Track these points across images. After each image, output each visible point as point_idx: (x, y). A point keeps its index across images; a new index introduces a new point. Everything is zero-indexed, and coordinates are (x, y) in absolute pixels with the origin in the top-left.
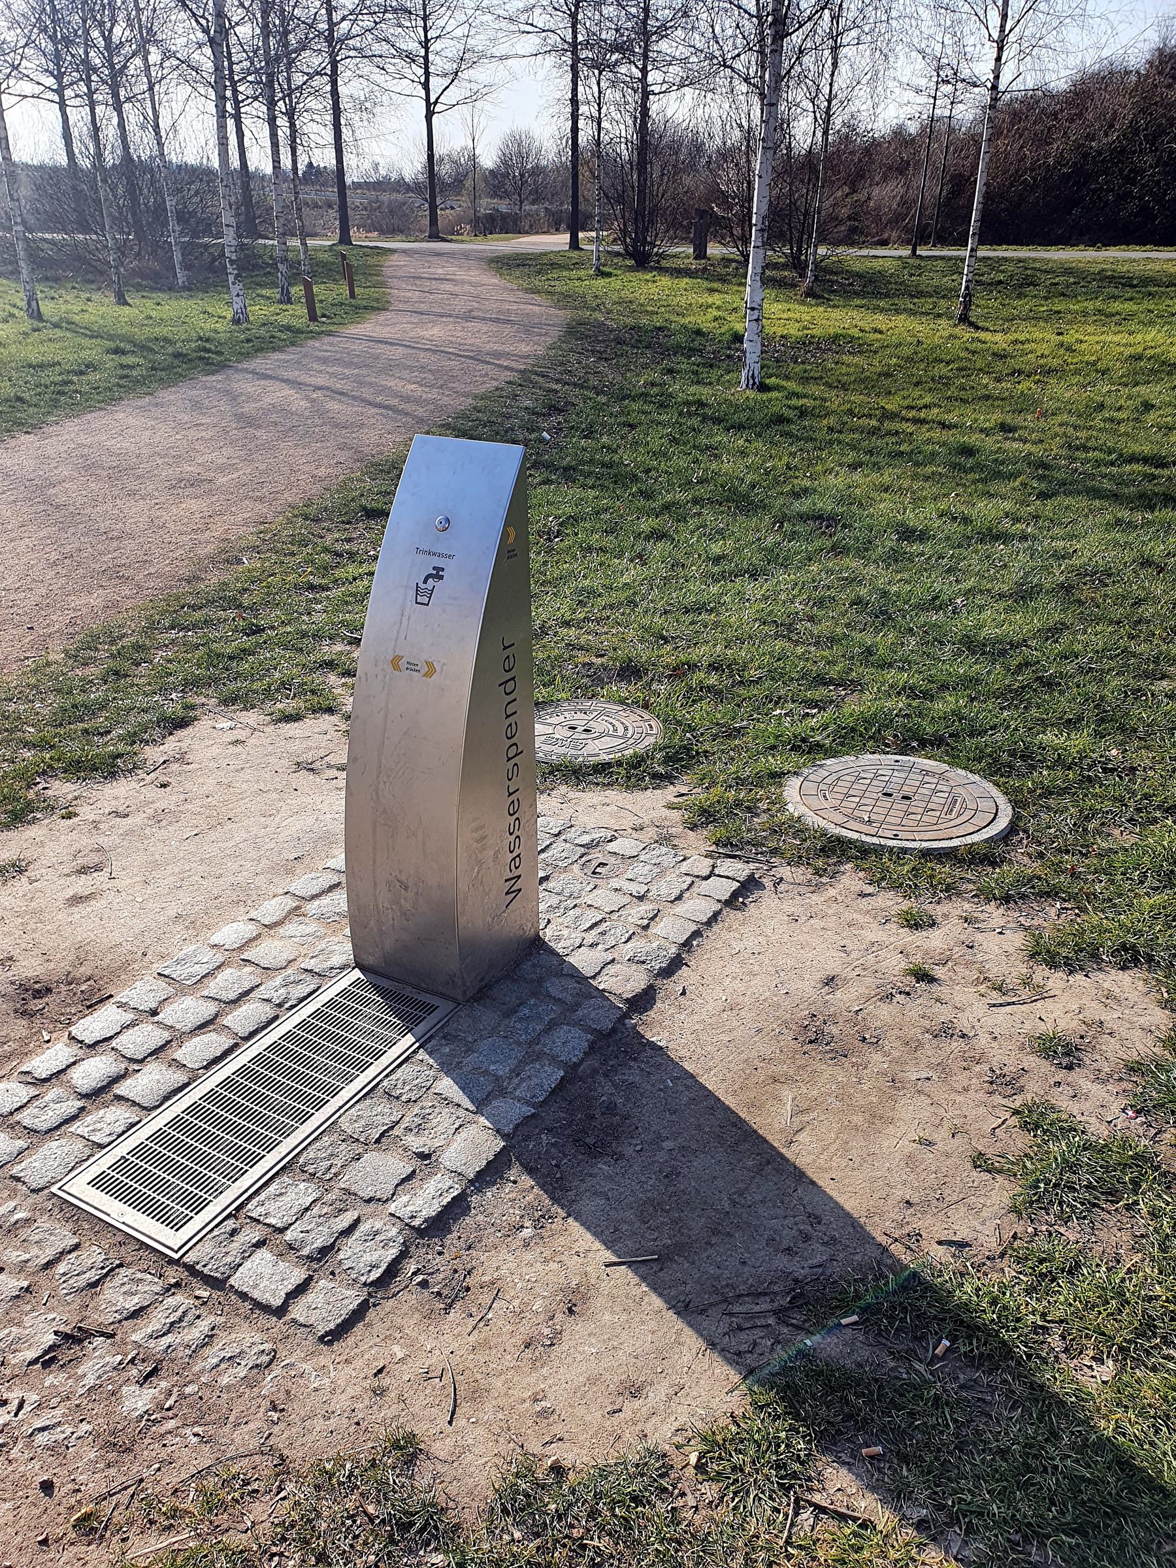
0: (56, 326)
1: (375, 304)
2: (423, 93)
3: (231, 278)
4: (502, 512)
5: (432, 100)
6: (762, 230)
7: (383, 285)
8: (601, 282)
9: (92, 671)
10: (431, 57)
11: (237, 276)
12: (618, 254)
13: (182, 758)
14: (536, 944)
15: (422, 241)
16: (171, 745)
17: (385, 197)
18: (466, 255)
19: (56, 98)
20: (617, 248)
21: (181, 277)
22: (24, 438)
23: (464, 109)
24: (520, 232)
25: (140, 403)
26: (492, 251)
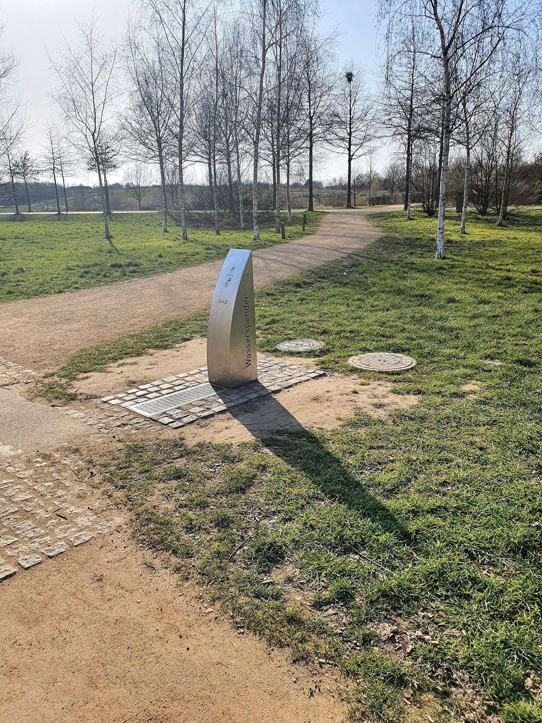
0: (192, 242)
1: (311, 233)
2: (348, 152)
3: (254, 224)
4: (244, 265)
5: (351, 154)
6: (443, 200)
7: (318, 226)
8: (409, 222)
9: (168, 329)
10: (352, 138)
11: (256, 223)
12: (420, 211)
13: (185, 346)
14: (256, 381)
15: (343, 209)
16: (183, 344)
17: (336, 192)
18: (359, 214)
19: (208, 162)
20: (420, 209)
21: (242, 225)
22: (169, 274)
23: (367, 157)
24: (391, 204)
25: (209, 264)
26: (371, 212)
